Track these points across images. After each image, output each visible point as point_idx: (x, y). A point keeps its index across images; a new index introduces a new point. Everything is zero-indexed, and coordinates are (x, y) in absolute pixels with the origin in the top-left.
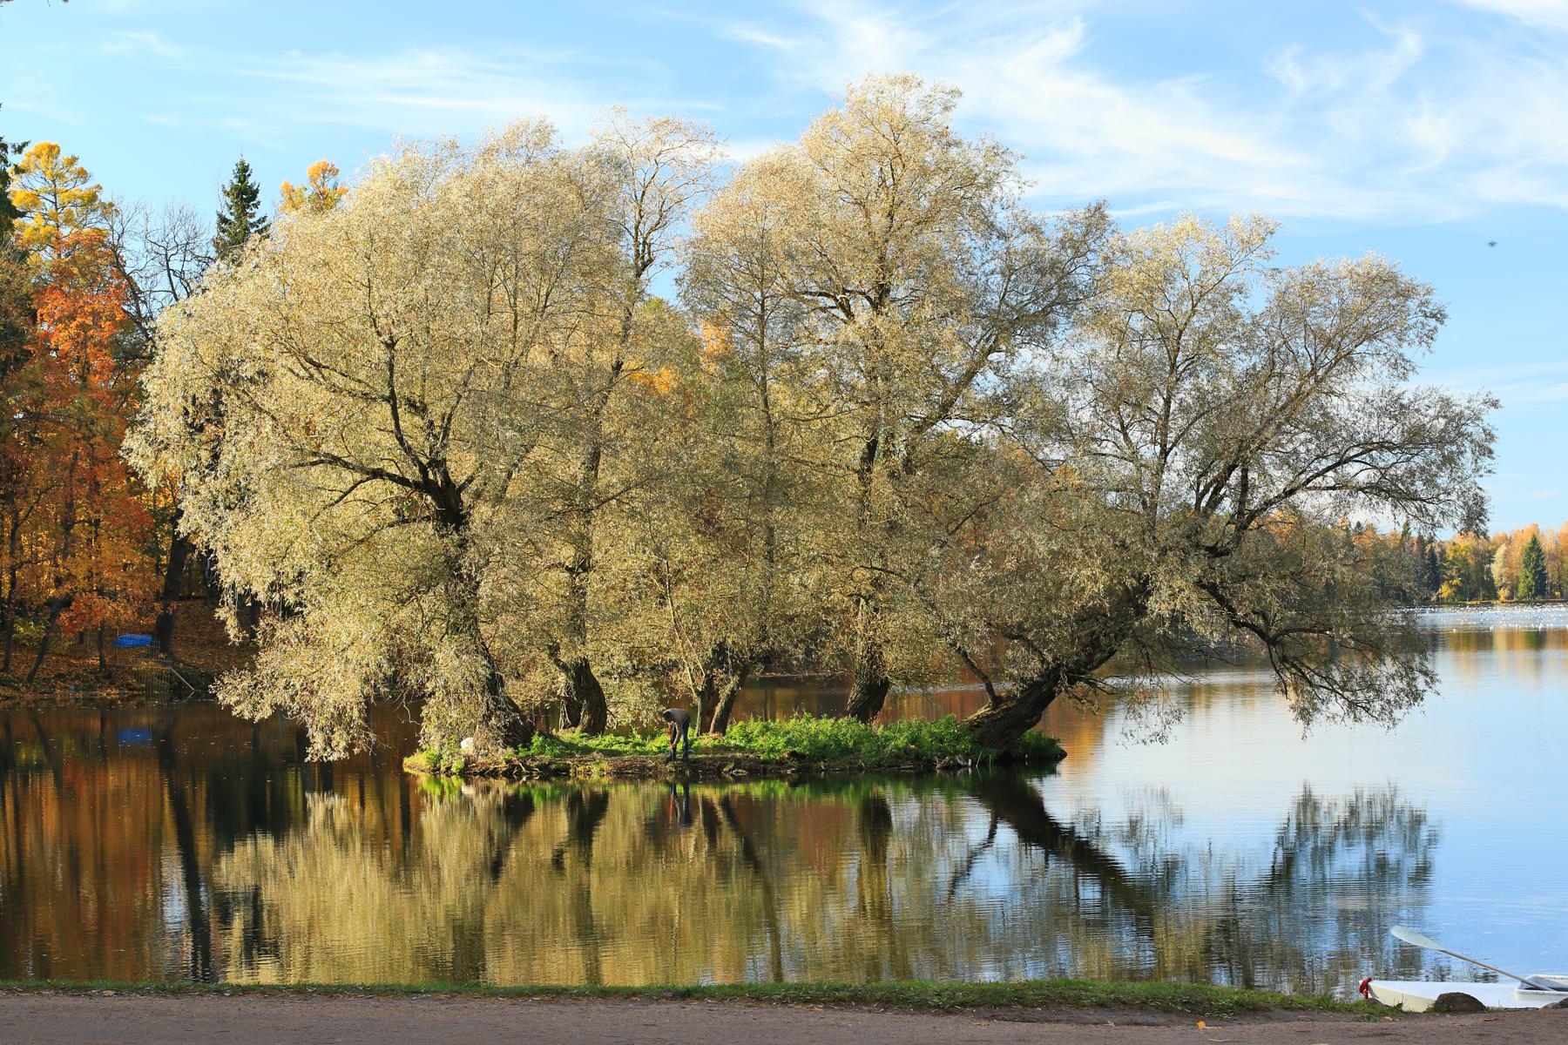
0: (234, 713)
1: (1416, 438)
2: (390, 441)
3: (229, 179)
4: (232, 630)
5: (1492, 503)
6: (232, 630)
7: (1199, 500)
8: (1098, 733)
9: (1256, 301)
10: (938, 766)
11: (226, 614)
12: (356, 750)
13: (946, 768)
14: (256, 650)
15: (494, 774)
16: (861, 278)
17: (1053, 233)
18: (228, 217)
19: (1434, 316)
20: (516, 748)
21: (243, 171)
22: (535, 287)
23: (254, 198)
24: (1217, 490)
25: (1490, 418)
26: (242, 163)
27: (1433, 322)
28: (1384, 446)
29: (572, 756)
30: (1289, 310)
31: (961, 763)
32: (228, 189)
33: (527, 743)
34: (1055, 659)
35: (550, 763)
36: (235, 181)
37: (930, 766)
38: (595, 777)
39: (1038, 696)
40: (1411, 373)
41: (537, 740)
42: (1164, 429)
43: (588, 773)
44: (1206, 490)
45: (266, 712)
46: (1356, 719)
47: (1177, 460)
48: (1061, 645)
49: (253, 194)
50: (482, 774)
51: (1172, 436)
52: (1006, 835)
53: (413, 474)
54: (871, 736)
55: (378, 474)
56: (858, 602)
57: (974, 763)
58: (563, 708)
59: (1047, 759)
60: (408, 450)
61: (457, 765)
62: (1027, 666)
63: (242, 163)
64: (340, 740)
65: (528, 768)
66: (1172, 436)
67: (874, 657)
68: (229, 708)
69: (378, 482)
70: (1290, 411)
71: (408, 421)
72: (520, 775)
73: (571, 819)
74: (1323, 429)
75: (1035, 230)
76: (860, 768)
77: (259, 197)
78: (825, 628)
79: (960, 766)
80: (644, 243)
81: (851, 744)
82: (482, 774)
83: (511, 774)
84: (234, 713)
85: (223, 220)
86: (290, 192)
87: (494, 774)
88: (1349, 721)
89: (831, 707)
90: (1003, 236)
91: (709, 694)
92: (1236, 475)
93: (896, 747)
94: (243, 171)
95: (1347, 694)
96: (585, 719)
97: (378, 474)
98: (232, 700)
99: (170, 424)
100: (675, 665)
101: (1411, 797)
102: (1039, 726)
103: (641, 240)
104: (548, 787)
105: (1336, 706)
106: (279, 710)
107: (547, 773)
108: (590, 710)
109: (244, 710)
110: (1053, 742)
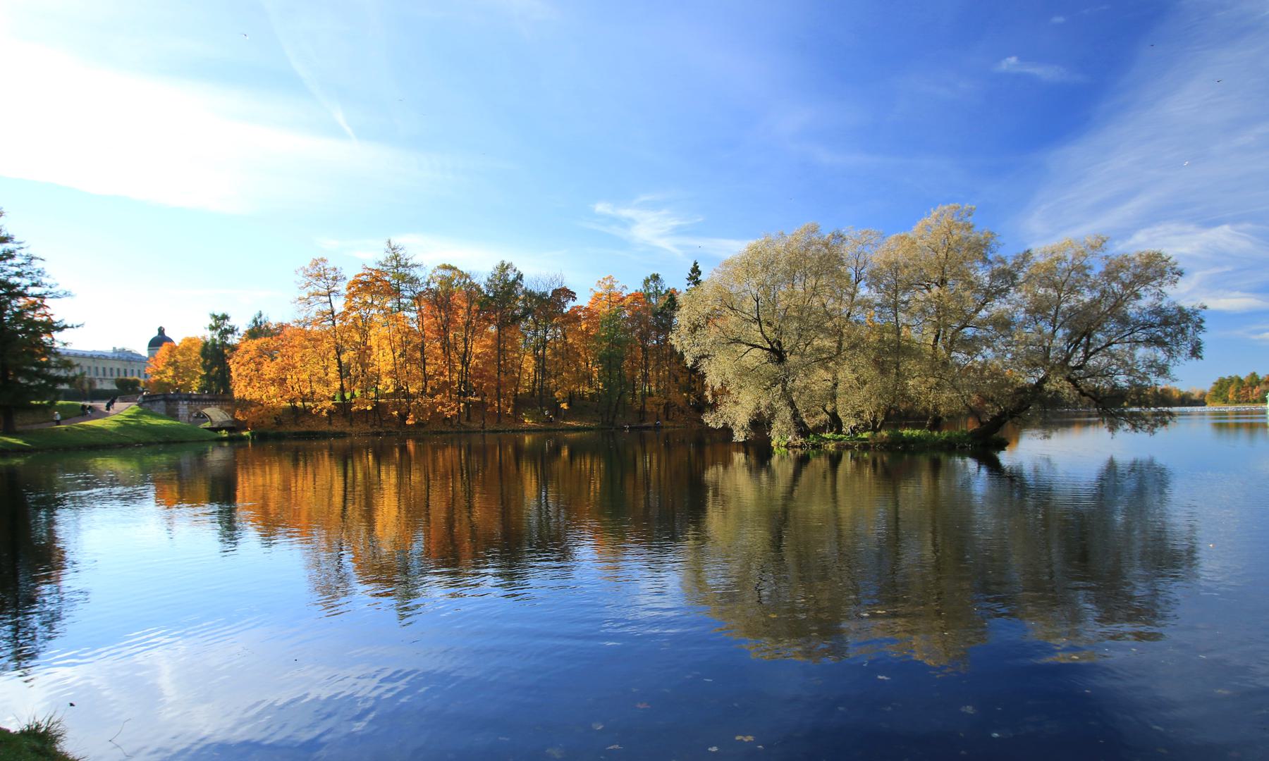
1: (1166, 322)
4: (710, 398)
5: (1205, 343)
6: (710, 398)
8: (1017, 440)
10: (957, 447)
11: (708, 393)
13: (961, 448)
15: (796, 447)
16: (935, 276)
17: (1010, 262)
19: (1177, 274)
22: (811, 281)
24: (1076, 345)
25: (1202, 313)
27: (1177, 276)
33: (808, 437)
34: (1004, 408)
37: (955, 446)
38: (830, 448)
39: (998, 422)
42: (1054, 321)
43: (828, 447)
44: (1071, 345)
46: (1136, 432)
47: (1060, 333)
48: (1007, 404)
50: (792, 447)
51: (1058, 324)
52: (984, 472)
53: (768, 346)
55: (755, 346)
56: (931, 391)
58: (828, 426)
59: (1002, 445)
60: (765, 336)
61: (784, 444)
62: (992, 411)
64: (743, 434)
65: (808, 445)
66: (1058, 324)
67: (935, 408)
68: (707, 424)
70: (1105, 317)
71: (765, 328)
72: (805, 447)
73: (568, 451)
74: (1124, 320)
75: (1003, 262)
78: (821, 254)
79: (966, 447)
82: (792, 447)
88: (1133, 432)
89: (921, 426)
90: (990, 263)
92: (1084, 340)
95: (1132, 422)
96: (835, 430)
97: (755, 346)
98: (709, 421)
99: (684, 331)
100: (863, 412)
101: (1160, 461)
102: (999, 433)
105: (1127, 426)
106: (725, 424)
107: (814, 447)
109: (713, 425)
110: (1004, 439)
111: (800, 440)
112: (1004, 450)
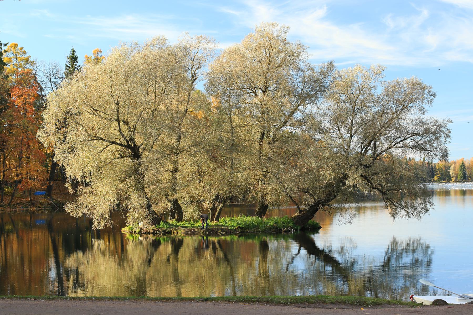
0: (70, 215)
1: (427, 132)
2: (117, 133)
3: (69, 54)
6: (70, 190)
7: (362, 151)
9: (379, 91)
11: (68, 185)
12: (107, 226)
13: (285, 231)
14: (77, 196)
15: (149, 233)
17: (318, 70)
18: (69, 65)
20: (156, 225)
21: (73, 51)
23: (76, 60)
24: (367, 148)
25: (449, 126)
26: (73, 49)
28: (417, 134)
29: (172, 228)
30: (389, 93)
31: (290, 230)
32: (69, 57)
34: (318, 199)
35: (166, 230)
36: (71, 55)
38: (179, 234)
39: (313, 210)
40: (425, 112)
41: (162, 223)
42: (351, 129)
43: (177, 233)
44: (364, 148)
45: (80, 215)
46: (409, 217)
47: (355, 139)
49: (76, 58)
50: (145, 233)
54: (262, 222)
56: (259, 181)
57: (294, 230)
59: (316, 229)
63: (73, 49)
64: (102, 223)
66: (353, 131)
67: (263, 198)
69: (114, 145)
75: (312, 69)
76: (259, 232)
77: (78, 59)
79: (289, 231)
80: (194, 73)
81: (256, 224)
83: (154, 233)
84: (70, 215)
85: (67, 66)
86: (87, 57)
87: (149, 233)
88: (407, 217)
90: (302, 71)
91: (214, 209)
93: (270, 225)
94: (73, 51)
97: (114, 143)
100: (203, 200)
101: (426, 240)
103: (193, 72)
104: (165, 237)
105: (403, 213)
106: (84, 214)
107: (165, 233)
108: (178, 214)
109: (73, 214)
111: (151, 228)
112: (318, 233)
